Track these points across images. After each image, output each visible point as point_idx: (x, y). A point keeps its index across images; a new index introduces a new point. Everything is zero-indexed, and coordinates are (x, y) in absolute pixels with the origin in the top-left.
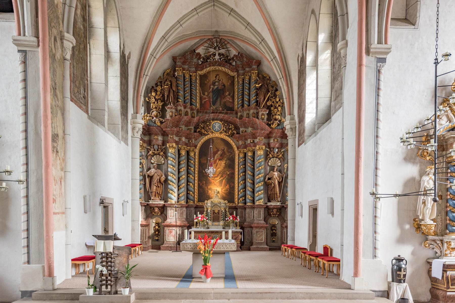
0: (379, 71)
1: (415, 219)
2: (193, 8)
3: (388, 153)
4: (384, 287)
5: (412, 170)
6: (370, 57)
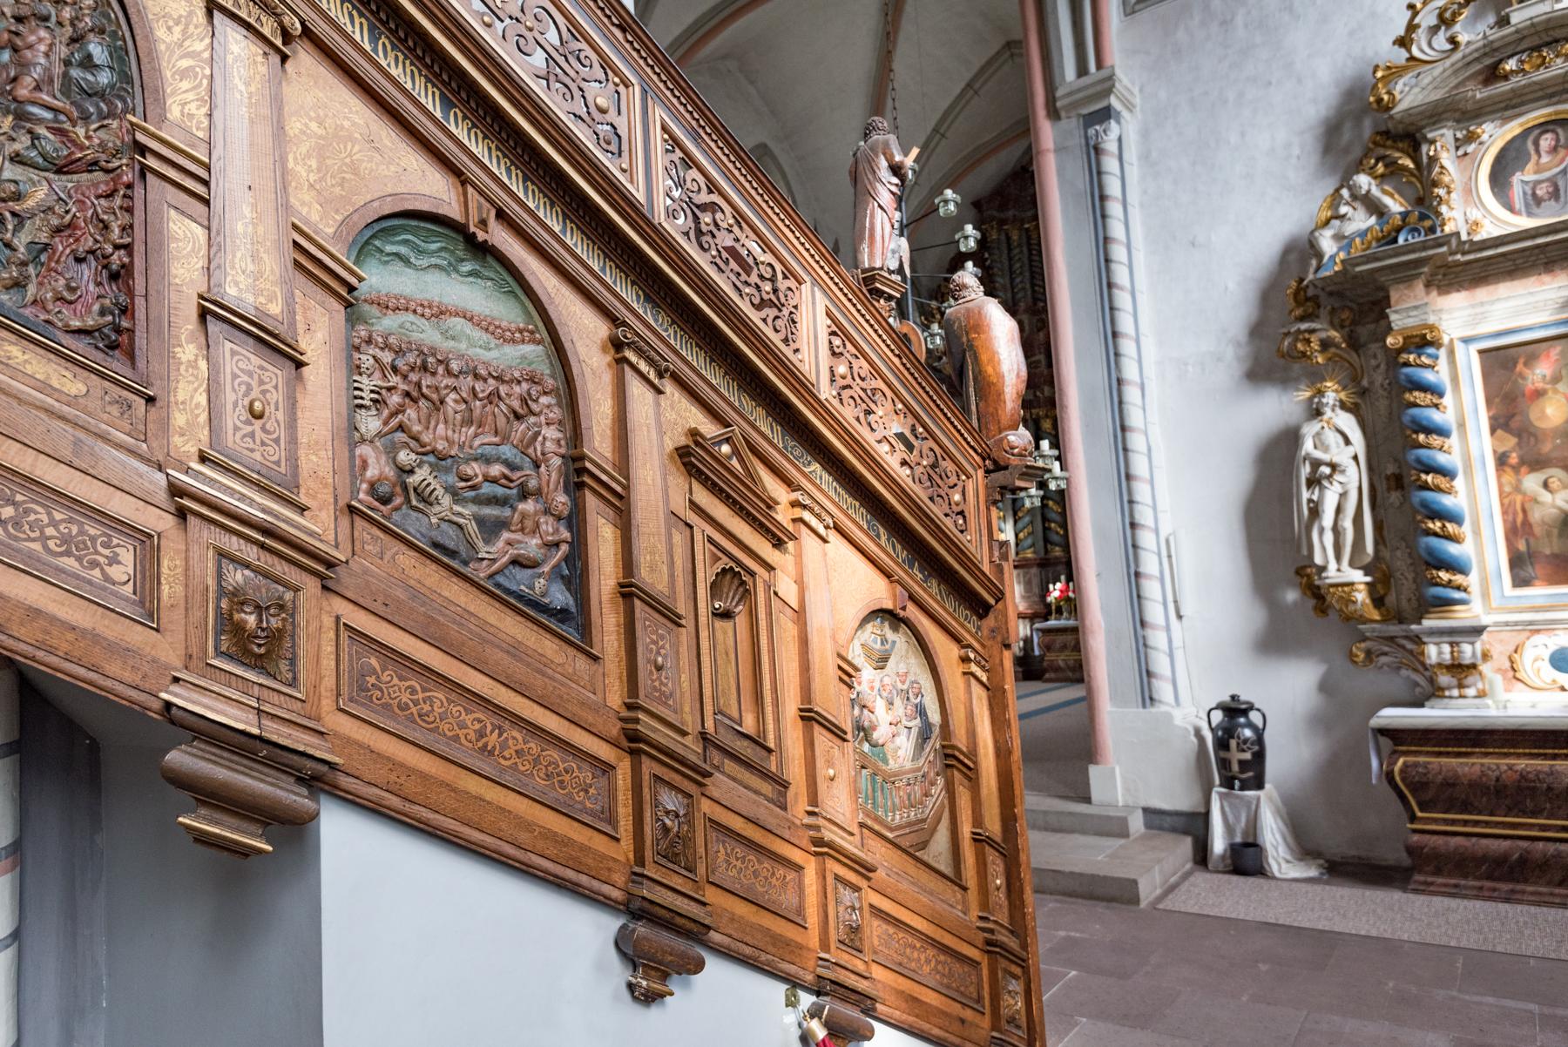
0: (1095, 151)
1: (1304, 567)
2: (962, 85)
3: (1190, 368)
4: (1179, 798)
5: (1274, 407)
6: (1064, 123)
